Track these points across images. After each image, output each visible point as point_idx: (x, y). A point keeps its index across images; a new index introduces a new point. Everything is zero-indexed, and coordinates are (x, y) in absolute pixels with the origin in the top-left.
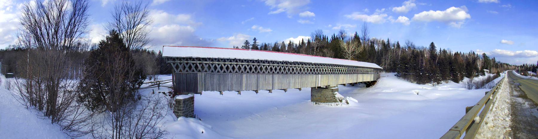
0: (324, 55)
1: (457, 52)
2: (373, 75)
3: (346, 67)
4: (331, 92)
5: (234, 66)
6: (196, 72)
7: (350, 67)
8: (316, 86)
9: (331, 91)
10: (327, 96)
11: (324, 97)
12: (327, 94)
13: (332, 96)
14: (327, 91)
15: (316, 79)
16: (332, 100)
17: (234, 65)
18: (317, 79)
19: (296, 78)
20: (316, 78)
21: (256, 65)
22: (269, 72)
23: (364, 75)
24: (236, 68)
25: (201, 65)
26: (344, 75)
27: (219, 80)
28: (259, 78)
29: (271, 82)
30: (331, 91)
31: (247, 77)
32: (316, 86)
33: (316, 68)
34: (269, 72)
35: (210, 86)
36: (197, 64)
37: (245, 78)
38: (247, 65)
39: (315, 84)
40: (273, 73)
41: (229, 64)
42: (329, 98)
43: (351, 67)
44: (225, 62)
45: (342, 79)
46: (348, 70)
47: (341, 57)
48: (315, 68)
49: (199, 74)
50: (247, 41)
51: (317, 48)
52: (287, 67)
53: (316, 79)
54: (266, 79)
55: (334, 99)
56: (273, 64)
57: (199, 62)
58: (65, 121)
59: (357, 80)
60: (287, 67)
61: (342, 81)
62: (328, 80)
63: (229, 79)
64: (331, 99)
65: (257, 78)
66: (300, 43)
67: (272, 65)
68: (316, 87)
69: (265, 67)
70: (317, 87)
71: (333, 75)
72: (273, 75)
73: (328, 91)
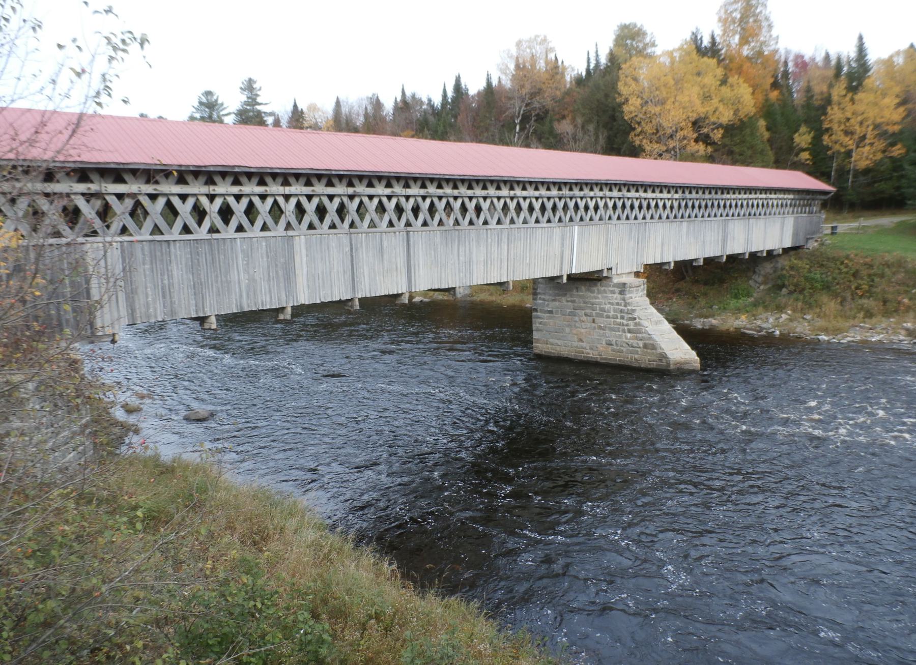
0: (554, 142)
1: (458, 87)
2: (790, 222)
3: (676, 192)
4: (617, 295)
5: (299, 200)
6: (69, 235)
7: (690, 193)
8: (561, 270)
9: (617, 290)
10: (603, 310)
11: (586, 315)
12: (600, 304)
13: (621, 311)
14: (599, 292)
15: (563, 245)
16: (620, 324)
17: (277, 198)
18: (567, 242)
19: (489, 240)
20: (563, 239)
21: (339, 196)
22: (456, 220)
23: (752, 221)
24: (264, 208)
25: (98, 204)
26: (667, 225)
27: (193, 268)
28: (357, 250)
29: (401, 261)
30: (617, 290)
31: (581, 234)
32: (561, 270)
33: (560, 198)
34: (456, 220)
35: (154, 300)
36: (107, 198)
37: (304, 252)
38: (207, 195)
39: (558, 263)
40: (408, 224)
41: (229, 195)
42: (608, 317)
43: (713, 192)
44: (212, 188)
45: (659, 241)
46: (683, 204)
47: (635, 152)
48: (557, 200)
49: (92, 248)
50: (208, 93)
51: (525, 119)
52: (263, 197)
53: (563, 245)
54: (381, 249)
55: (631, 322)
56: (404, 187)
57: (82, 187)
58: (195, 405)
59: (724, 241)
60: (263, 197)
61: (659, 251)
62: (606, 245)
63: (240, 262)
64: (618, 320)
65: (348, 249)
66: (445, 91)
67: (404, 193)
68: (560, 277)
69: (270, 201)
70: (565, 278)
71: (623, 225)
72: (408, 232)
73: (605, 292)
